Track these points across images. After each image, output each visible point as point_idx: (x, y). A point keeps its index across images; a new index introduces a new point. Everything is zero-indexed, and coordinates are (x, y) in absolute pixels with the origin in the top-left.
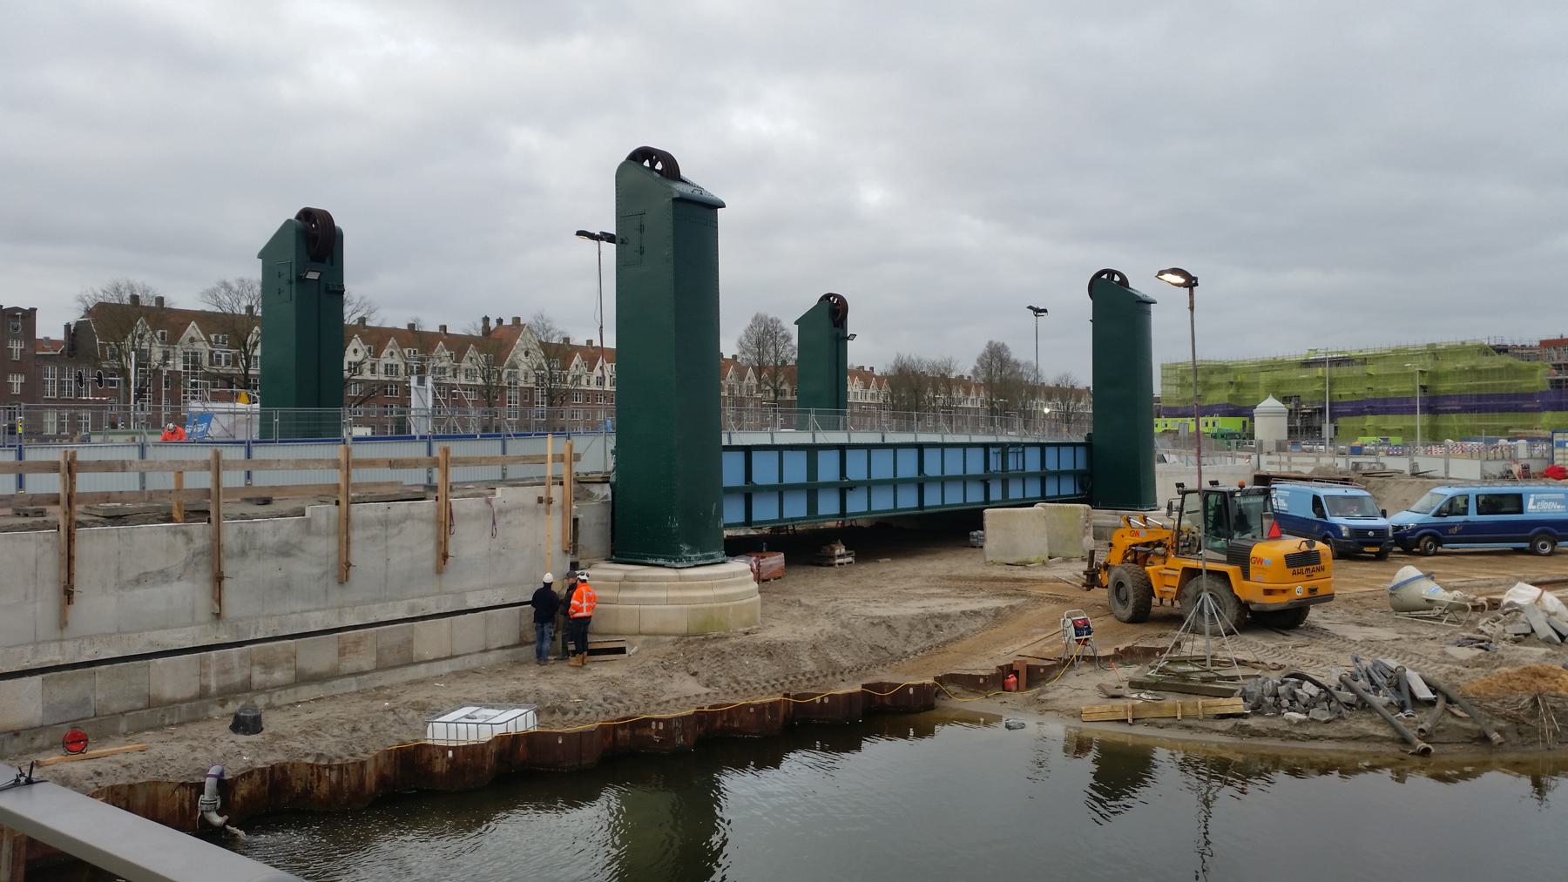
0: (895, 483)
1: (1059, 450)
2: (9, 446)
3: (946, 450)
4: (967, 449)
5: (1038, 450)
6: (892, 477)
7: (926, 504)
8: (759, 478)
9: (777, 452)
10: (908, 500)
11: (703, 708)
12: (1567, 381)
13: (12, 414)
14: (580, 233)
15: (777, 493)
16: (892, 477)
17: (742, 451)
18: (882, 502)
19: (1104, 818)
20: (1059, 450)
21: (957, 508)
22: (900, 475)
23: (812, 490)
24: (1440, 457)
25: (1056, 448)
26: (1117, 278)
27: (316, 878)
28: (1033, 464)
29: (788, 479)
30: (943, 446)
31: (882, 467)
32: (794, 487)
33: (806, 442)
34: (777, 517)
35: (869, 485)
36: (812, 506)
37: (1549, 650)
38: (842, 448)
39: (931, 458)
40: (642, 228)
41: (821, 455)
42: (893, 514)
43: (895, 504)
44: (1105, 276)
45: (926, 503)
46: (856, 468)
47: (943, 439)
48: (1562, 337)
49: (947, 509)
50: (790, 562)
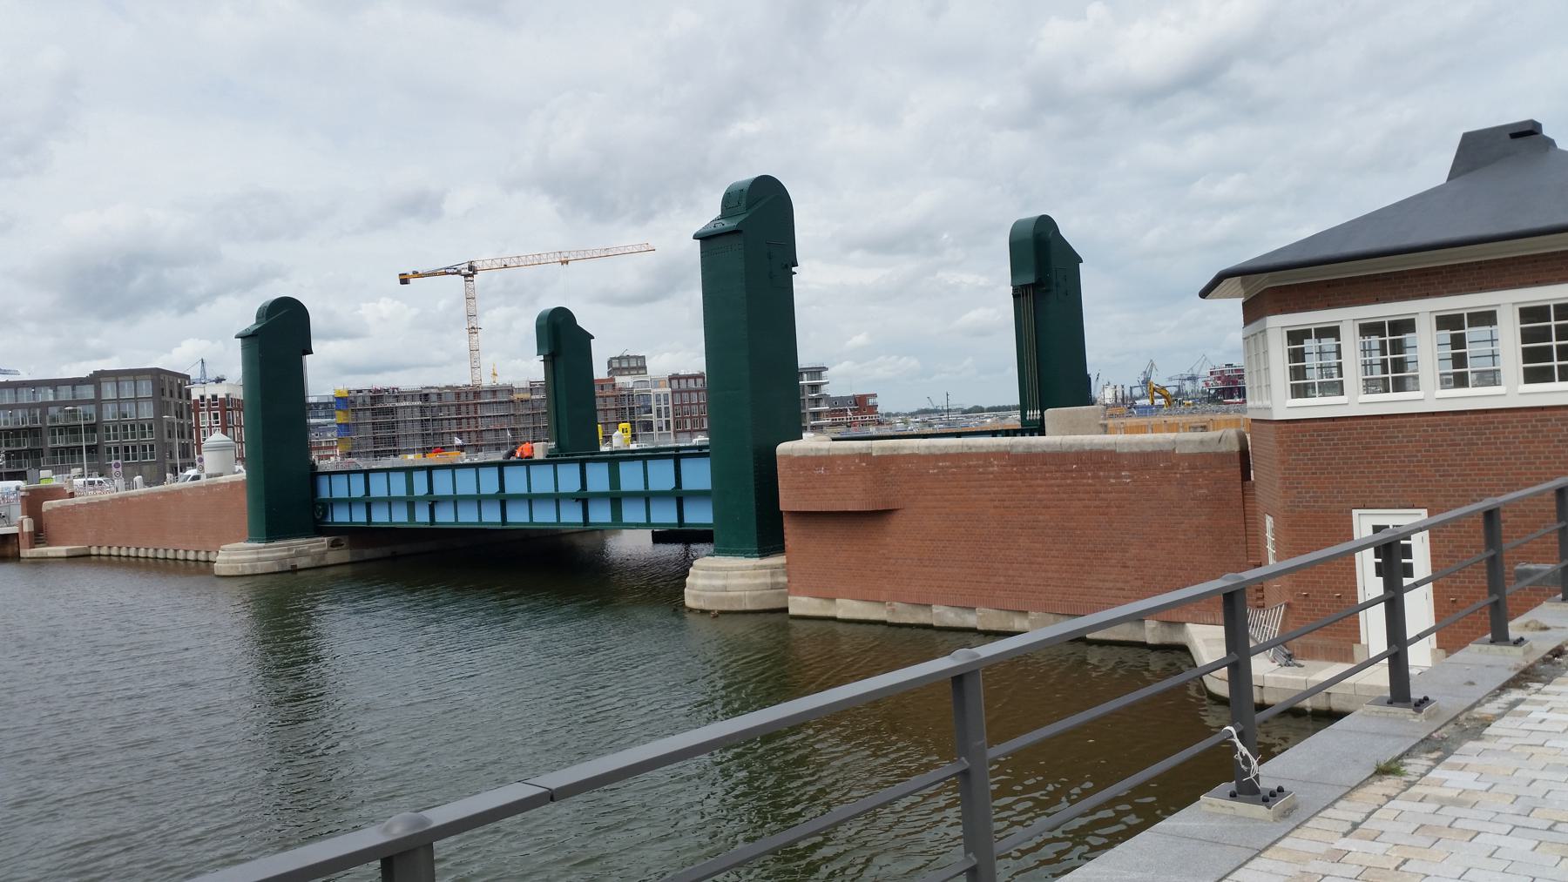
1: (330, 478)
3: (351, 475)
4: (456, 470)
5: (424, 474)
6: (476, 493)
8: (374, 493)
9: (552, 466)
10: (491, 516)
12: (1566, 310)
14: (1528, 786)
15: (644, 500)
16: (476, 493)
18: (468, 516)
19: (501, 878)
20: (330, 478)
22: (562, 490)
23: (411, 503)
29: (654, 486)
30: (453, 467)
32: (489, 498)
34: (388, 521)
36: (411, 514)
38: (430, 469)
39: (420, 480)
42: (476, 526)
45: (591, 520)
46: (443, 485)
49: (483, 527)
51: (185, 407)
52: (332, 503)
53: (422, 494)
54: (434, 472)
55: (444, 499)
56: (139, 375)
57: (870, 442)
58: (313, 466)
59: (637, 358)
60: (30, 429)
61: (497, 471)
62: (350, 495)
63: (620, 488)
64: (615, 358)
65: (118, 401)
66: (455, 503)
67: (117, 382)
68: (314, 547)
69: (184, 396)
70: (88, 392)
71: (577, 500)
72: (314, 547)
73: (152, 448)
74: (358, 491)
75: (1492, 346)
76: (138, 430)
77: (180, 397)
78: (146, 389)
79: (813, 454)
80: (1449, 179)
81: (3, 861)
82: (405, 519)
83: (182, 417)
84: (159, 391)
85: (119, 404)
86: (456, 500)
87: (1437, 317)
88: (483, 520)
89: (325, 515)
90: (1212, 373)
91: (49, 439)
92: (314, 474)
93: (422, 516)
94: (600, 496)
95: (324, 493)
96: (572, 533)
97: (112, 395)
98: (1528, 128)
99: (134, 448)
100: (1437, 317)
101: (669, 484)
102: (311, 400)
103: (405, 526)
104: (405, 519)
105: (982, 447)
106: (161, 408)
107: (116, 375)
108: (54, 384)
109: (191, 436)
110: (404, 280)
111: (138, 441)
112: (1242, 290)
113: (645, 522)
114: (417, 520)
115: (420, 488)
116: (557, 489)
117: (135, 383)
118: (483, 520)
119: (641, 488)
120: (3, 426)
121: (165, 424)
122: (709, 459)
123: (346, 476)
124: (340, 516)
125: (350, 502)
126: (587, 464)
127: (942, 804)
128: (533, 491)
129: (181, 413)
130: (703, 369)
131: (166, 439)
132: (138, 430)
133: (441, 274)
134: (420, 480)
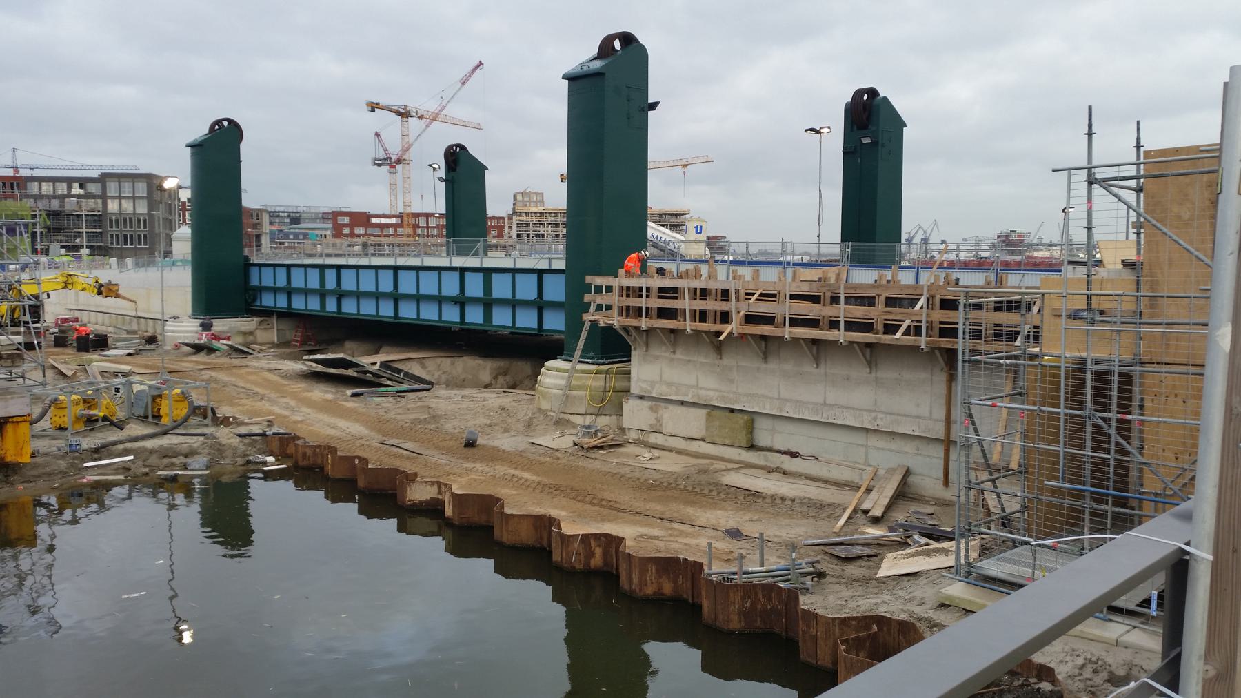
0: (440, 300)
2: (959, 269)
3: (360, 271)
10: (386, 310)
11: (353, 395)
17: (397, 273)
18: (314, 305)
21: (371, 318)
22: (444, 293)
24: (490, 218)
26: (225, 123)
27: (1093, 693)
28: (314, 283)
31: (429, 285)
32: (526, 304)
33: (390, 264)
34: (375, 313)
36: (488, 316)
39: (331, 276)
42: (374, 318)
43: (306, 306)
44: (217, 127)
46: (349, 283)
47: (396, 262)
48: (655, 672)
52: (261, 289)
53: (332, 288)
54: (399, 271)
56: (122, 178)
57: (267, 263)
58: (246, 258)
59: (536, 194)
61: (458, 275)
63: (491, 296)
64: (519, 193)
66: (377, 299)
67: (119, 182)
68: (244, 326)
71: (456, 303)
72: (244, 326)
76: (135, 222)
78: (142, 189)
82: (318, 308)
85: (100, 197)
86: (359, 295)
88: (361, 312)
89: (255, 300)
90: (999, 237)
92: (247, 265)
93: (331, 306)
94: (475, 301)
95: (254, 282)
97: (115, 193)
101: (533, 295)
103: (317, 313)
104: (318, 308)
106: (152, 205)
111: (135, 231)
113: (511, 325)
114: (494, 323)
115: (331, 284)
116: (440, 292)
117: (134, 184)
118: (380, 314)
119: (436, 293)
122: (564, 275)
123: (374, 271)
124: (267, 301)
125: (275, 290)
126: (466, 273)
127: (675, 544)
128: (380, 290)
130: (445, 212)
132: (135, 222)
134: (331, 276)
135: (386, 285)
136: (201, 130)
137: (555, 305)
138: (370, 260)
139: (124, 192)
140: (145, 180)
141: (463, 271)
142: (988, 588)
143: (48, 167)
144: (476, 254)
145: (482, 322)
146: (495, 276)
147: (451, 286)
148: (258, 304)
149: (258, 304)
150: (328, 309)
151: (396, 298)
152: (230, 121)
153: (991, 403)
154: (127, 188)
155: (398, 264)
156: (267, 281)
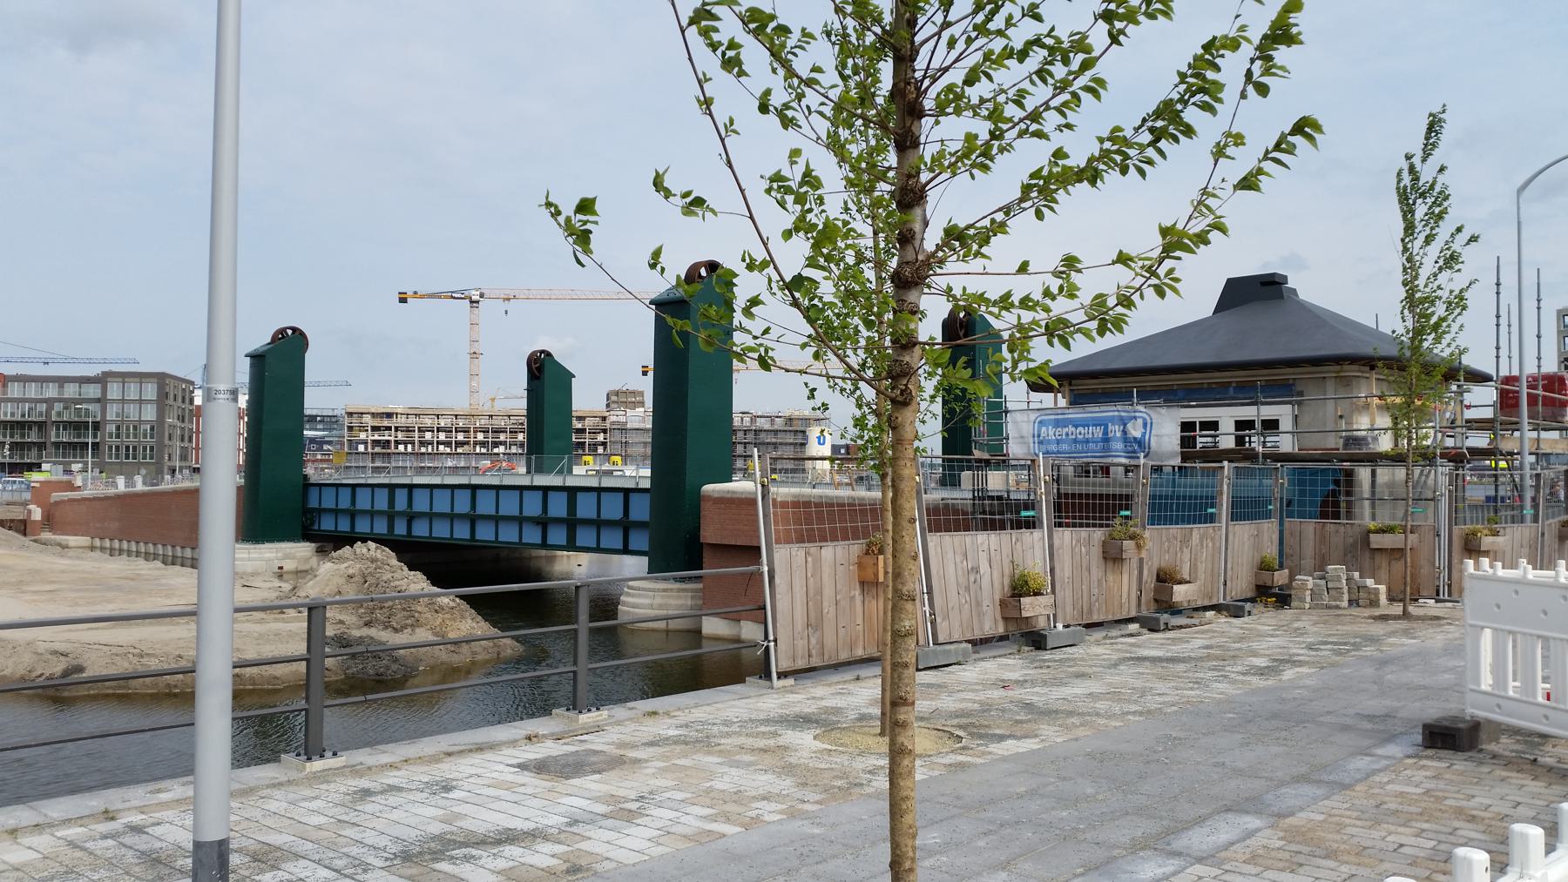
0: (452, 517)
5: (405, 491)
7: (413, 534)
10: (462, 532)
13: (186, 438)
14: (1233, 159)
18: (441, 531)
22: (456, 511)
23: (391, 516)
25: (518, 492)
26: (290, 332)
28: (382, 503)
34: (428, 535)
35: (431, 516)
37: (84, 675)
39: (401, 496)
40: (707, 103)
41: (398, 491)
43: (521, 538)
50: (653, 569)
51: (187, 411)
52: (321, 511)
54: (524, 492)
55: (421, 515)
60: (18, 422)
62: (497, 512)
65: (123, 401)
67: (141, 383)
69: (187, 401)
70: (93, 391)
71: (538, 524)
73: (152, 449)
74: (345, 503)
75: (1538, 440)
77: (183, 402)
78: (150, 391)
79: (729, 496)
80: (1219, 309)
81: (3, 872)
83: (183, 421)
84: (163, 395)
87: (1236, 422)
88: (455, 536)
89: (313, 523)
91: (53, 433)
92: (307, 485)
94: (558, 521)
96: (485, 547)
98: (1270, 279)
99: (135, 448)
100: (1236, 422)
101: (617, 514)
102: (307, 412)
105: (734, 492)
107: (124, 377)
108: (62, 381)
109: (190, 440)
110: (403, 300)
112: (1531, 369)
115: (401, 503)
116: (521, 512)
118: (455, 536)
119: (448, 510)
120: (3, 418)
121: (167, 426)
125: (336, 512)
129: (183, 417)
131: (166, 442)
133: (446, 297)
134: (401, 496)
135: (463, 505)
136: (261, 338)
137: (641, 525)
138: (564, 480)
139: (129, 396)
140: (156, 380)
141: (546, 490)
142: (94, 698)
143: (67, 361)
144: (560, 472)
145: (386, 532)
146: (580, 495)
147: (533, 507)
148: (316, 527)
149: (316, 527)
150: (396, 532)
151: (473, 519)
152: (294, 330)
153: (1123, 601)
154: (132, 392)
155: (415, 482)
156: (328, 503)
